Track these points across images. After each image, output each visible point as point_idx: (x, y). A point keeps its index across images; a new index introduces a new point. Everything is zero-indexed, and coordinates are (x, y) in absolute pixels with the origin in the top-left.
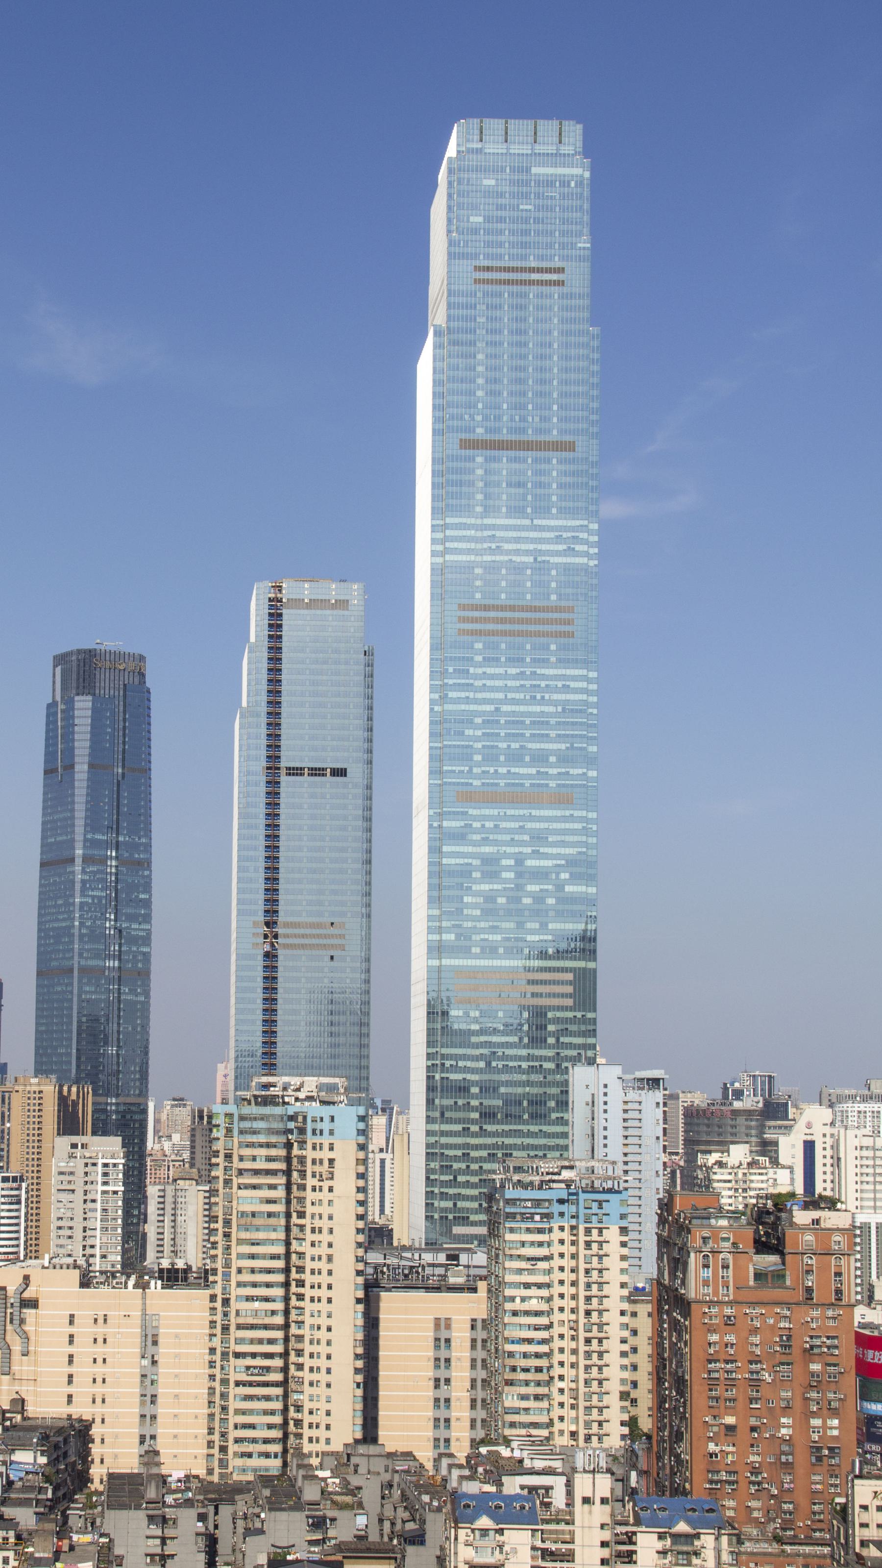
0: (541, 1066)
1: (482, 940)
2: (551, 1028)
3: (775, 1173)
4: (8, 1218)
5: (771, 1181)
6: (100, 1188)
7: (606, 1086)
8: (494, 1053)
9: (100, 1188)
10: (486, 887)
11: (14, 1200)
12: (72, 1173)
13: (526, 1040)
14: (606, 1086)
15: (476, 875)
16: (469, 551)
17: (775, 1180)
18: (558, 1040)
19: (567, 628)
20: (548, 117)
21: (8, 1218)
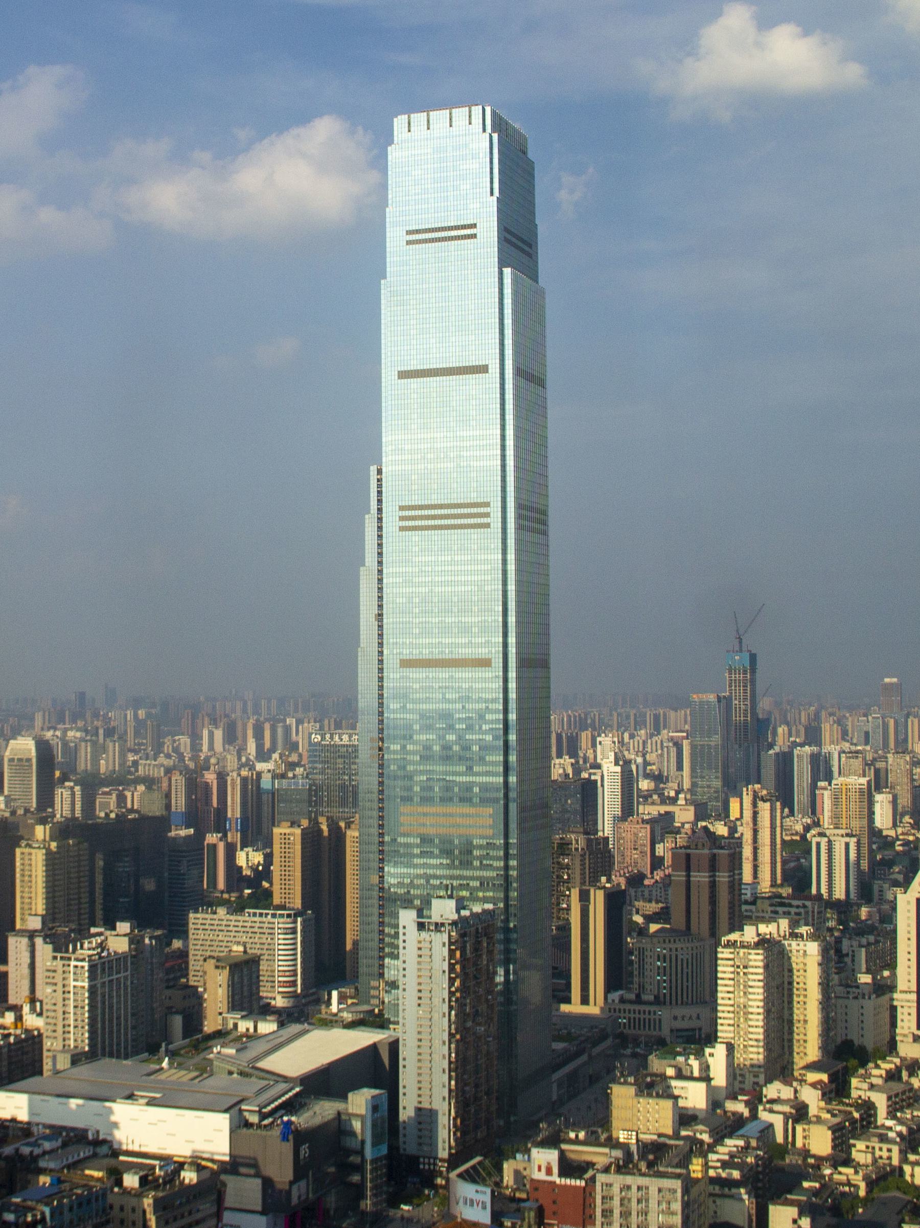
0: (468, 884)
1: (480, 740)
2: (476, 853)
3: (805, 945)
4: (284, 944)
5: (802, 952)
6: (73, 983)
7: (404, 927)
8: (488, 854)
9: (73, 983)
10: (423, 737)
11: (292, 973)
12: (55, 971)
13: (457, 862)
14: (404, 927)
15: (416, 727)
16: (103, 1042)
17: (805, 951)
18: (481, 863)
19: (485, 520)
20: (440, 107)
21: (284, 944)
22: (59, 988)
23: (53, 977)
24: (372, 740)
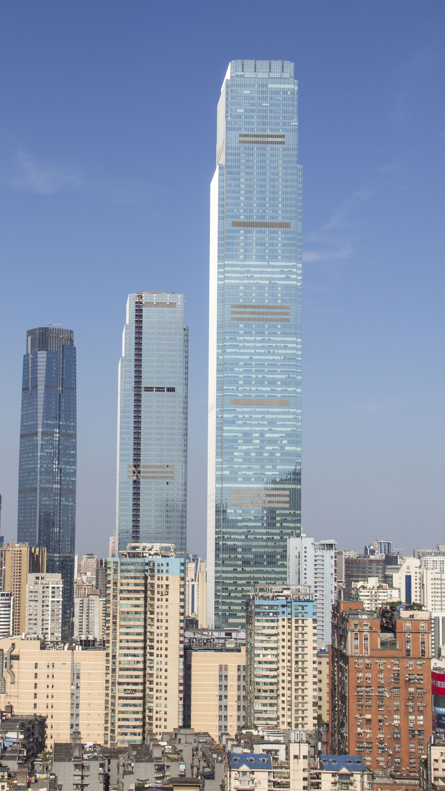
0: (273, 538)
2: (278, 518)
3: (391, 592)
4: (4, 614)
5: (389, 596)
6: (51, 599)
7: (306, 548)
9: (51, 599)
10: (245, 447)
12: (36, 592)
13: (265, 525)
14: (306, 548)
15: (240, 441)
17: (391, 595)
18: (281, 525)
20: (276, 59)
21: (4, 614)
22: (40, 603)
23: (35, 596)
24: (129, 466)
